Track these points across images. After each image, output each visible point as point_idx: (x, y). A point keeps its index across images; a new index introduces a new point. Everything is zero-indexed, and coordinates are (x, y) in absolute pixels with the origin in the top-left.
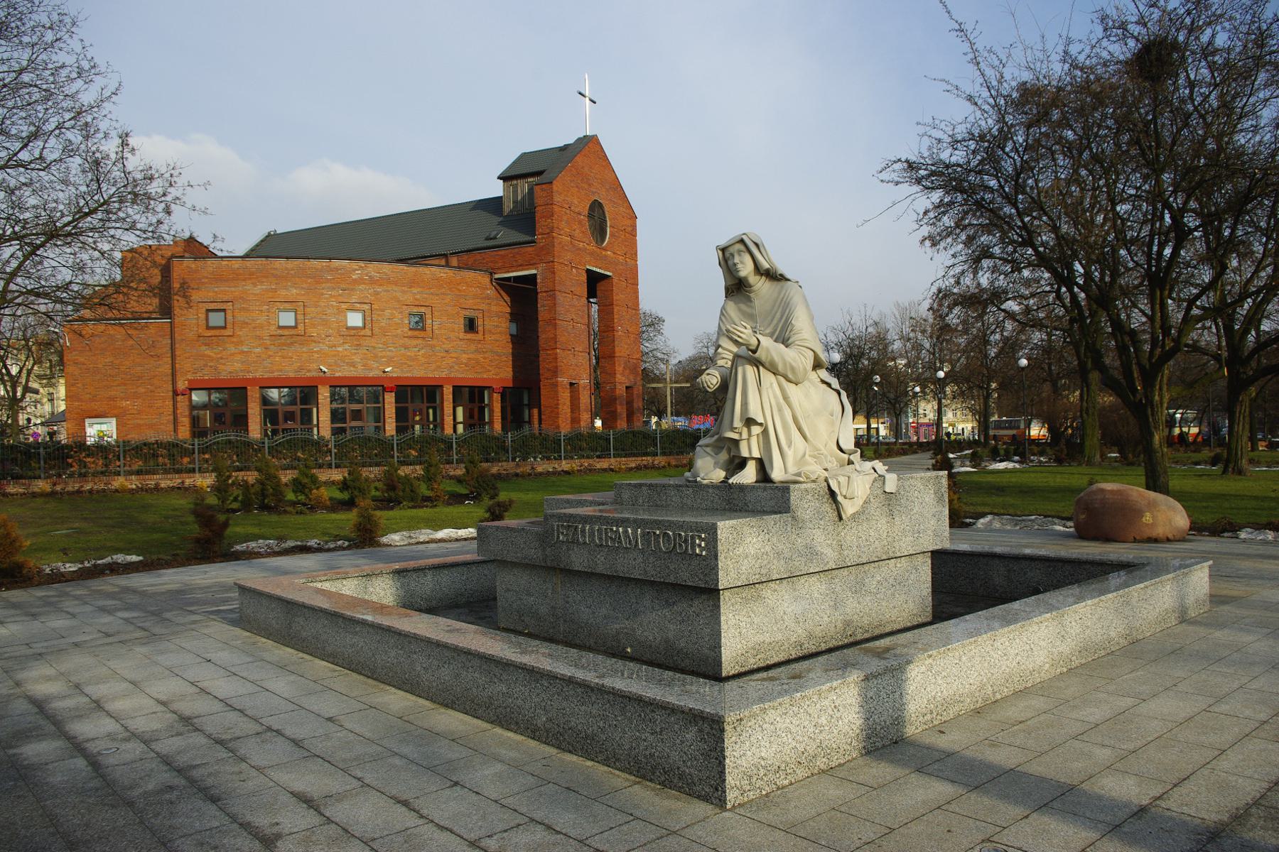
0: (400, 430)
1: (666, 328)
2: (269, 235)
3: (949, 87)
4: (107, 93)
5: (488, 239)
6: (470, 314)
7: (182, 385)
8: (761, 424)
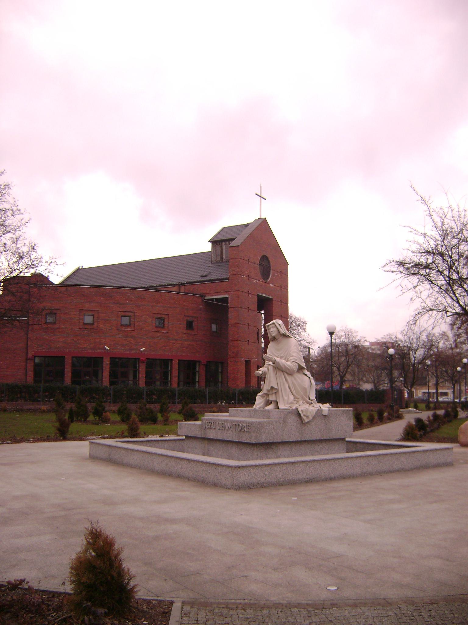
0: (147, 384)
1: (307, 327)
2: (78, 270)
3: (412, 230)
4: (23, 222)
5: (202, 276)
6: (189, 319)
7: (31, 354)
8: (276, 389)
